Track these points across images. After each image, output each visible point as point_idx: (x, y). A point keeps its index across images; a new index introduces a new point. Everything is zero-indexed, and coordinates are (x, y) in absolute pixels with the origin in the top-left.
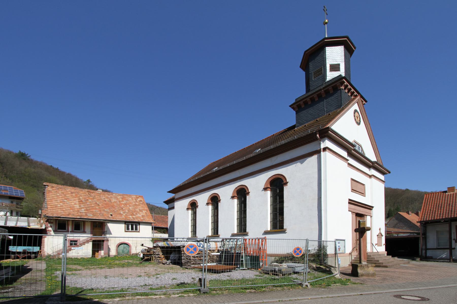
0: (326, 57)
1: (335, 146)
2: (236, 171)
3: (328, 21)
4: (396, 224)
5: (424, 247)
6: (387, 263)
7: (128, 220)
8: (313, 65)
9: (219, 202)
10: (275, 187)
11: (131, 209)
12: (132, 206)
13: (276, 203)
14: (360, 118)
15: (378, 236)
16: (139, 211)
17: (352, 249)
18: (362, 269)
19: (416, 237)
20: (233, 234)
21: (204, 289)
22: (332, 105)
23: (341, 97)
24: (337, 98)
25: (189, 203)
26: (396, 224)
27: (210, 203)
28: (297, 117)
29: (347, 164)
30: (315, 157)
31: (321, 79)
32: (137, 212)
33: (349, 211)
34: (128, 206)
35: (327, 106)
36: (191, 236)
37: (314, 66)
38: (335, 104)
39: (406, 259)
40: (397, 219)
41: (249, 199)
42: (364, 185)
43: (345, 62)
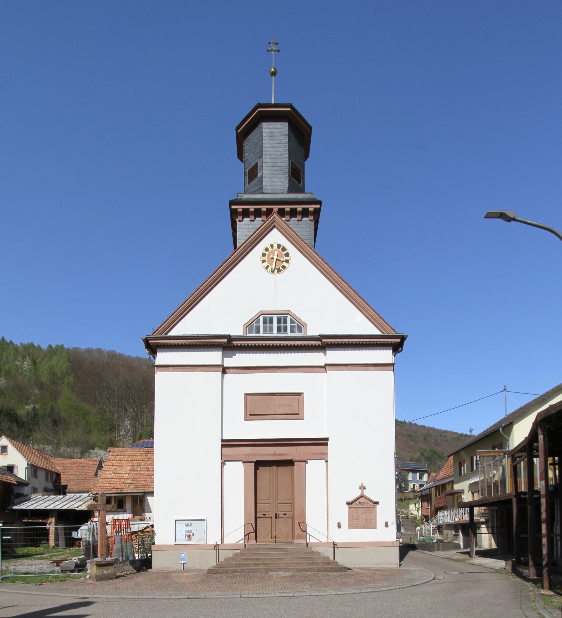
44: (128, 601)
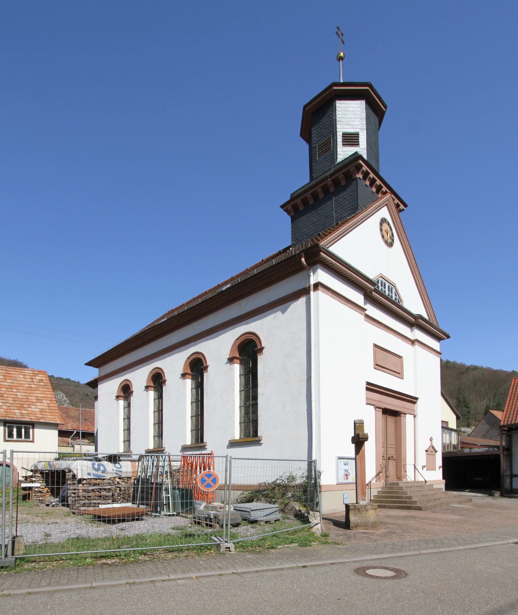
0: (336, 119)
1: (337, 281)
2: (189, 325)
3: (344, 54)
4: (487, 432)
5: (508, 473)
6: (425, 501)
7: (11, 419)
8: (317, 131)
9: (163, 385)
10: (247, 357)
11: (19, 397)
12: (23, 391)
13: (248, 387)
14: (392, 234)
15: (427, 451)
16: (35, 401)
17: (375, 474)
18: (357, 514)
19: (493, 454)
20: (184, 445)
21: (7, 560)
22: (344, 207)
23: (357, 193)
24: (351, 195)
25: (120, 385)
26: (487, 432)
27: (151, 386)
28: (294, 228)
29: (363, 317)
30: (302, 300)
31: (329, 160)
32: (31, 403)
33: (367, 404)
34: (14, 390)
35: (336, 209)
36: (124, 450)
37: (320, 135)
38: (349, 205)
39: (482, 494)
40: (488, 422)
41: (209, 378)
42: (402, 357)
43: (367, 129)
44: (96, 479)
